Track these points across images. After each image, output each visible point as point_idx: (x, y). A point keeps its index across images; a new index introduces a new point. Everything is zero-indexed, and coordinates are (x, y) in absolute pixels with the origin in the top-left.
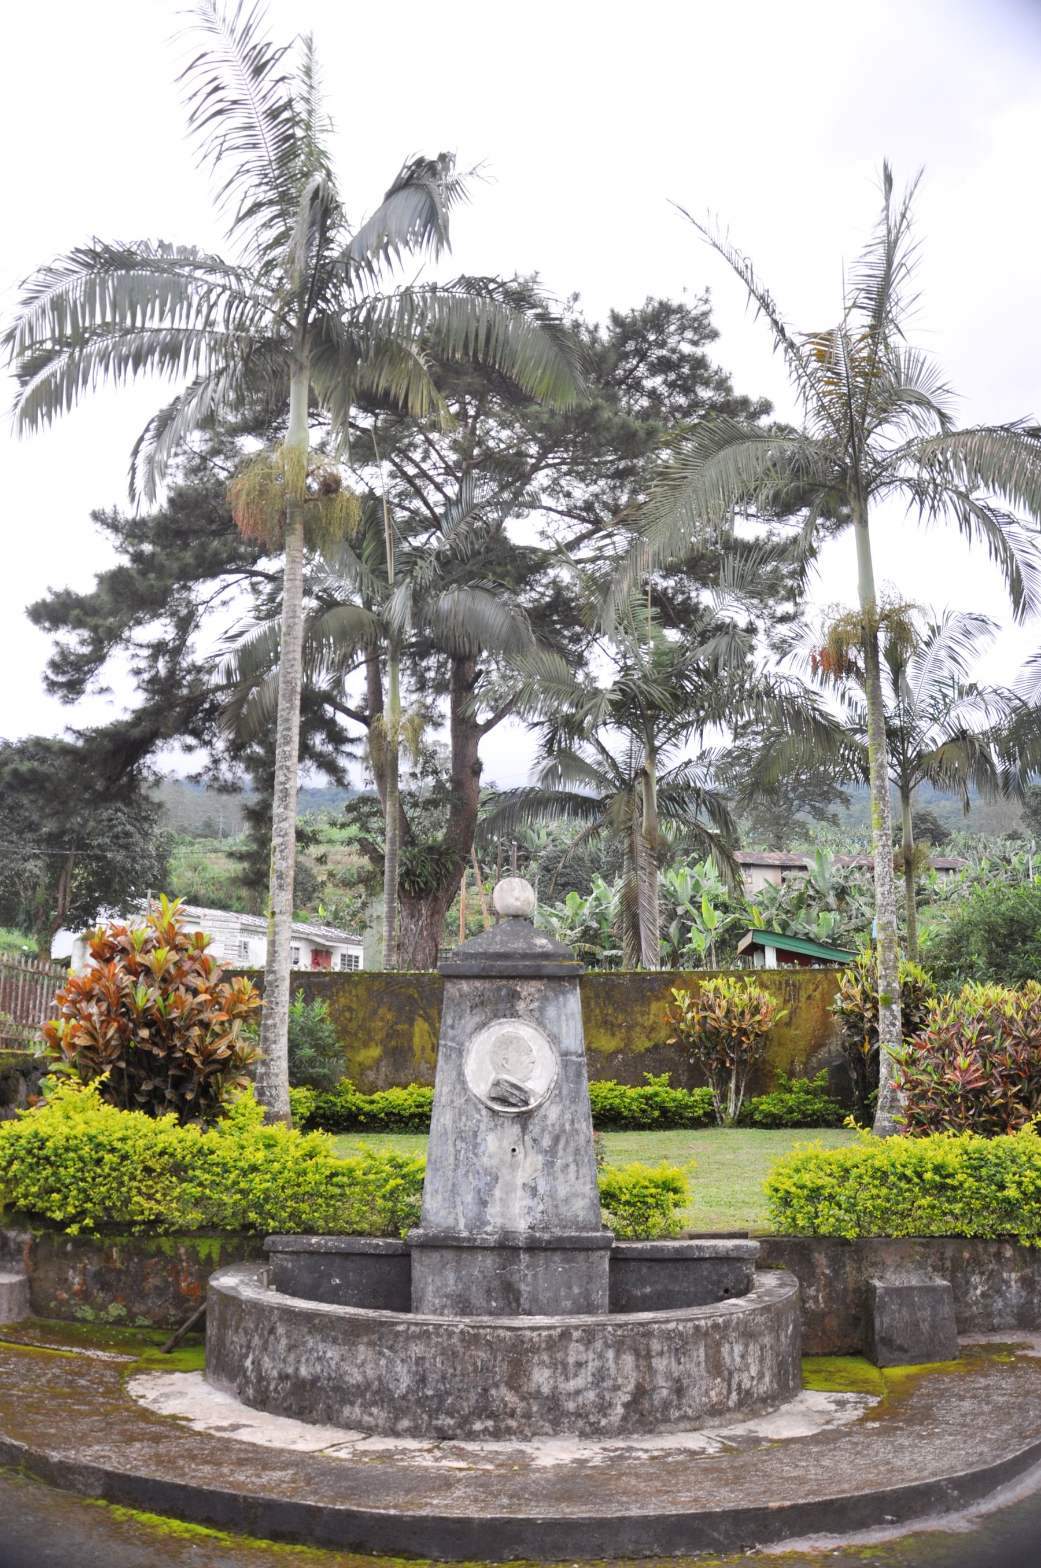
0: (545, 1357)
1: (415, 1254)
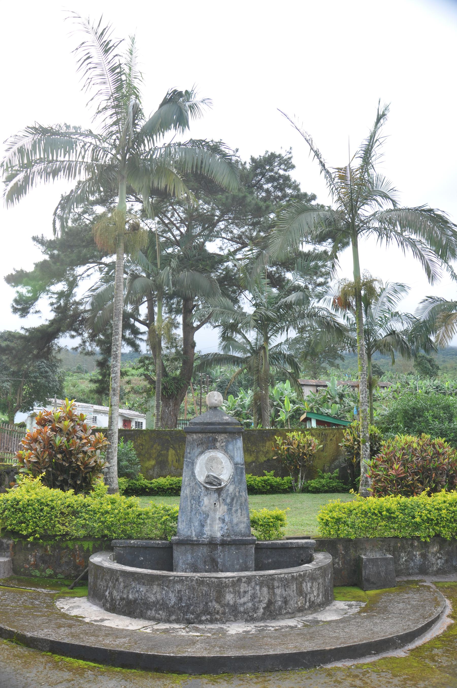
0: (231, 590)
1: (175, 547)
